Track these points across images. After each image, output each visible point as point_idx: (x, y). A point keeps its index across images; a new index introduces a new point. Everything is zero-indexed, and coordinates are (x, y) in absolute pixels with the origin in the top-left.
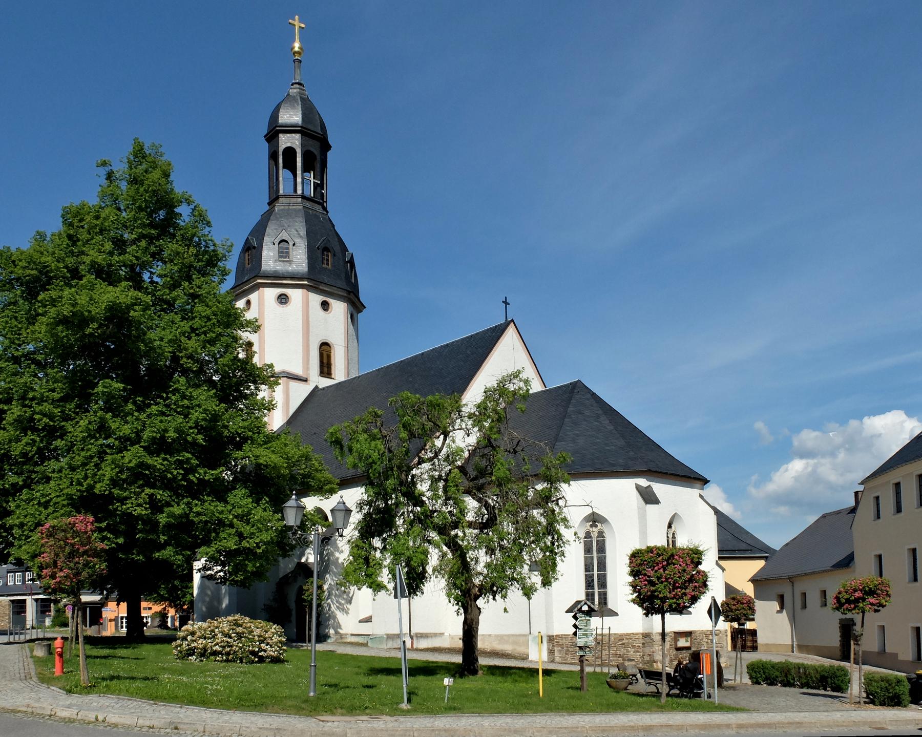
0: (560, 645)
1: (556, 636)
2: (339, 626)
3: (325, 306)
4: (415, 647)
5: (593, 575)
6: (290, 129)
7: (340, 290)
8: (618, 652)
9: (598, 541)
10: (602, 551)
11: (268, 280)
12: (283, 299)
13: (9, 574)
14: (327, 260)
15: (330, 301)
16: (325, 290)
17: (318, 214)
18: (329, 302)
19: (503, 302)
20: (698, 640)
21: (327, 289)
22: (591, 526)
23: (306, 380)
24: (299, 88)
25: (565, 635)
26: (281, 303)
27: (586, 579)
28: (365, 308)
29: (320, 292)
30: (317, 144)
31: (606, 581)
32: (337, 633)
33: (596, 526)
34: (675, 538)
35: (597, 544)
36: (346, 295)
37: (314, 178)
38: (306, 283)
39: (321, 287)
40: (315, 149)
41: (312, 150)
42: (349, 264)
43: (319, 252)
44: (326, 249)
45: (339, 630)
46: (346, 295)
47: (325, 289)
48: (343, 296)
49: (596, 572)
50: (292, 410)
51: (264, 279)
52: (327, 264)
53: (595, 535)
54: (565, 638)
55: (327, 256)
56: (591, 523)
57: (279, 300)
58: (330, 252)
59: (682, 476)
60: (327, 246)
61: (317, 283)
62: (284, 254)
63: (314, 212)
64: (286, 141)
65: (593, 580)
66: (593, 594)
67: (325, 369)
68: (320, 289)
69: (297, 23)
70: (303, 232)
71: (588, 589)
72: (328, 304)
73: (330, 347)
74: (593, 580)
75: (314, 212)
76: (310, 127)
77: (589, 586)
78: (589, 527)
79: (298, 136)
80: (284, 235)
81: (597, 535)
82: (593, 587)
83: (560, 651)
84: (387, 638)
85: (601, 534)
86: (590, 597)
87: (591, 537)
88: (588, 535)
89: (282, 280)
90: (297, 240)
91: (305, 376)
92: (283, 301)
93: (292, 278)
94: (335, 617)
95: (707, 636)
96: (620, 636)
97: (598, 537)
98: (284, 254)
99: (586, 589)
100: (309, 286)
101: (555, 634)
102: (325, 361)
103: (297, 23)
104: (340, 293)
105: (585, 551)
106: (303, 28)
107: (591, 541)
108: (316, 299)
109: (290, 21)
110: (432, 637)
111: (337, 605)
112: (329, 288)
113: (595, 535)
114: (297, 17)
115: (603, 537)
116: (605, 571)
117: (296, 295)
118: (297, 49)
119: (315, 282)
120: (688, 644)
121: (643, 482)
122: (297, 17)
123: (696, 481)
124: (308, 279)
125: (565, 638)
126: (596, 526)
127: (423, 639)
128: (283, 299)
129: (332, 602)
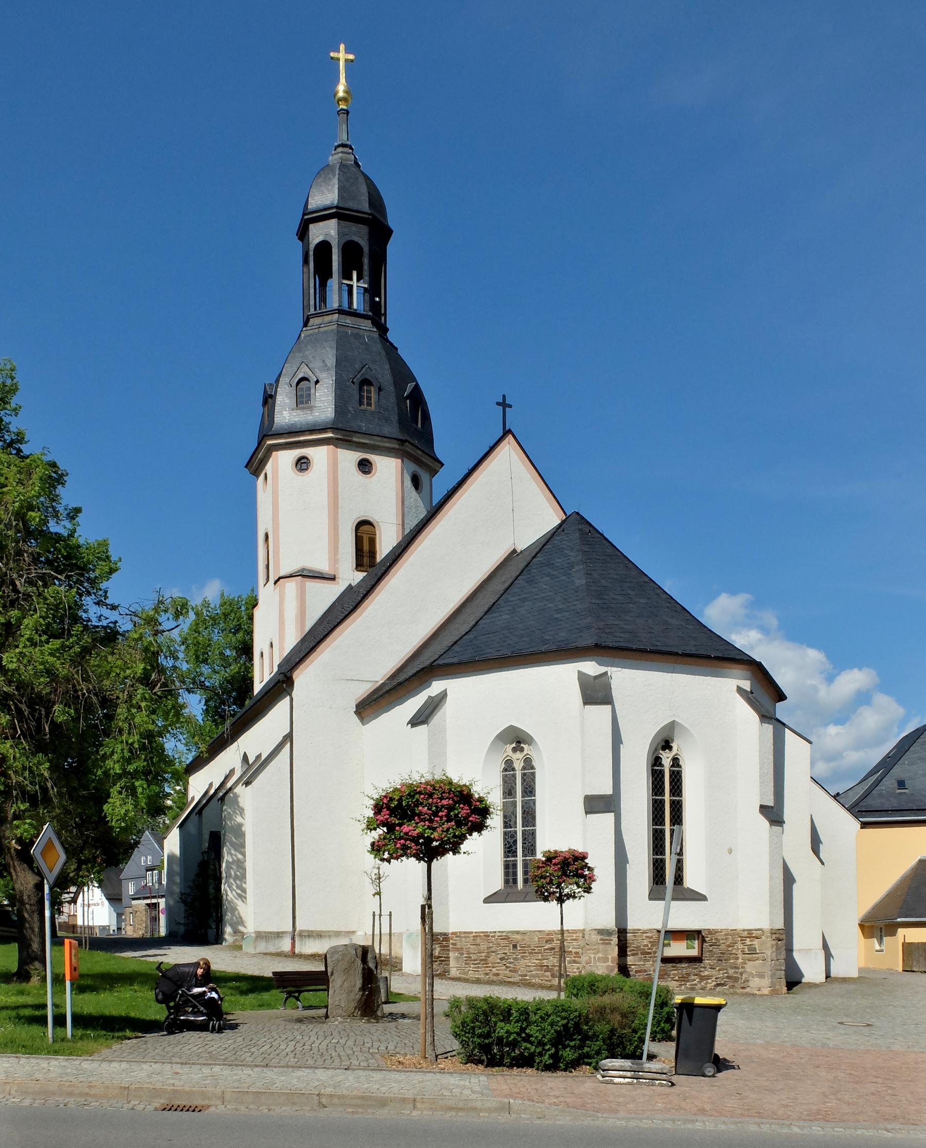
0: (458, 950)
1: (453, 933)
2: (241, 922)
3: (365, 466)
4: (297, 951)
5: (516, 832)
6: (322, 216)
7: (385, 440)
8: (545, 962)
9: (524, 775)
10: (531, 792)
11: (280, 438)
12: (302, 464)
13: (148, 873)
14: (369, 398)
15: (373, 458)
16: (365, 444)
17: (361, 332)
18: (371, 460)
19: (510, 406)
20: (723, 946)
21: (365, 441)
22: (514, 750)
23: (333, 579)
24: (342, 152)
25: (465, 933)
26: (301, 470)
27: (505, 839)
28: (443, 465)
29: (357, 447)
30: (364, 229)
31: (535, 842)
32: (236, 932)
33: (522, 750)
34: (679, 766)
35: (523, 780)
36: (397, 446)
37: (358, 281)
38: (331, 435)
39: (354, 439)
40: (360, 235)
41: (356, 239)
42: (408, 401)
43: (356, 387)
44: (366, 382)
45: (241, 928)
46: (397, 446)
47: (362, 441)
48: (393, 449)
49: (519, 829)
50: (309, 624)
51: (276, 439)
52: (369, 404)
53: (518, 765)
54: (465, 937)
55: (369, 392)
56: (514, 745)
57: (299, 466)
58: (373, 385)
59: (716, 658)
60: (368, 377)
61: (350, 433)
62: (302, 400)
63: (356, 331)
64: (320, 232)
65: (515, 841)
66: (515, 866)
67: (366, 560)
68: (355, 442)
69: (342, 55)
70: (331, 361)
71: (508, 857)
72: (371, 463)
73: (374, 527)
74: (515, 842)
75: (356, 331)
76: (351, 205)
77: (509, 852)
78: (510, 752)
79: (333, 222)
80: (304, 372)
81: (522, 764)
82: (514, 854)
83: (457, 958)
84: (257, 937)
85: (528, 763)
86: (511, 870)
87: (514, 769)
88: (509, 766)
89: (299, 436)
90: (323, 376)
91: (333, 573)
92: (304, 466)
93: (312, 431)
94: (234, 909)
95: (743, 939)
96: (548, 934)
97: (524, 768)
98: (302, 400)
99: (505, 857)
100: (337, 439)
101: (451, 931)
102: (366, 547)
103: (342, 55)
104: (387, 445)
105: (504, 793)
106: (352, 61)
107: (514, 776)
108: (349, 458)
109: (332, 54)
110: (330, 936)
111: (239, 891)
112: (370, 439)
113: (518, 765)
114: (342, 47)
115: (533, 768)
116: (534, 825)
117: (319, 455)
118: (341, 94)
119: (343, 432)
120: (694, 952)
121: (591, 668)
122: (342, 47)
123: (730, 665)
124: (333, 429)
125: (465, 937)
126: (522, 750)
127: (311, 940)
128: (302, 464)
129: (229, 887)
